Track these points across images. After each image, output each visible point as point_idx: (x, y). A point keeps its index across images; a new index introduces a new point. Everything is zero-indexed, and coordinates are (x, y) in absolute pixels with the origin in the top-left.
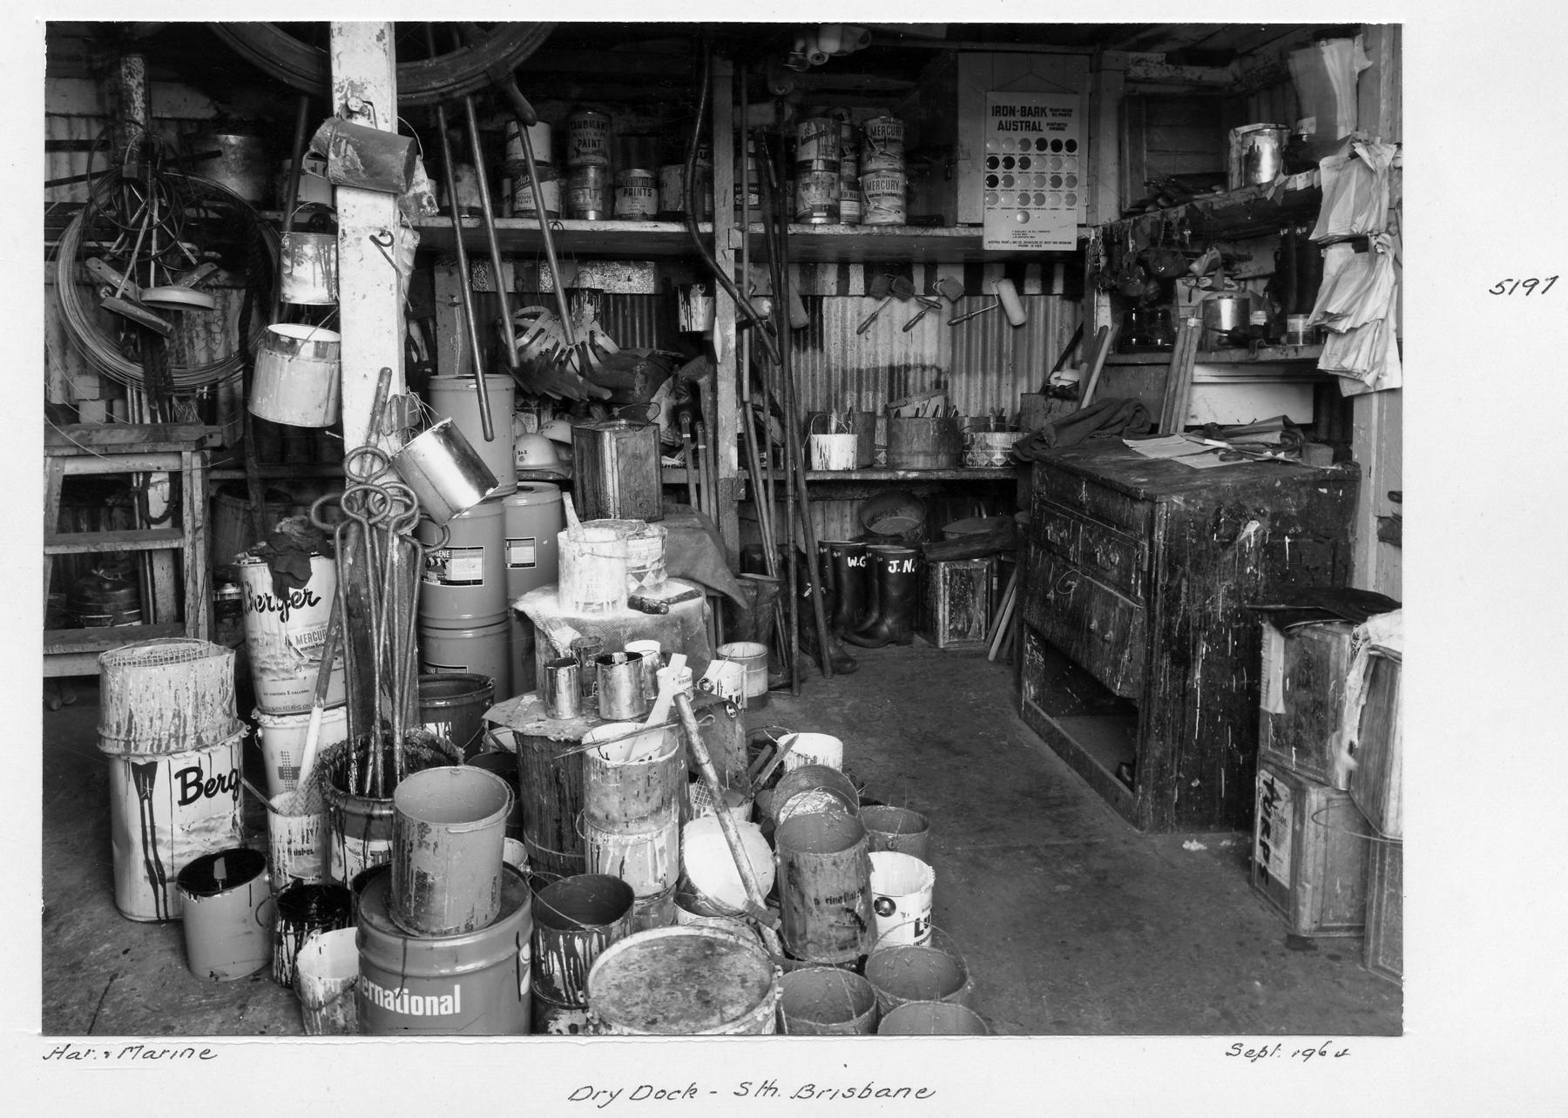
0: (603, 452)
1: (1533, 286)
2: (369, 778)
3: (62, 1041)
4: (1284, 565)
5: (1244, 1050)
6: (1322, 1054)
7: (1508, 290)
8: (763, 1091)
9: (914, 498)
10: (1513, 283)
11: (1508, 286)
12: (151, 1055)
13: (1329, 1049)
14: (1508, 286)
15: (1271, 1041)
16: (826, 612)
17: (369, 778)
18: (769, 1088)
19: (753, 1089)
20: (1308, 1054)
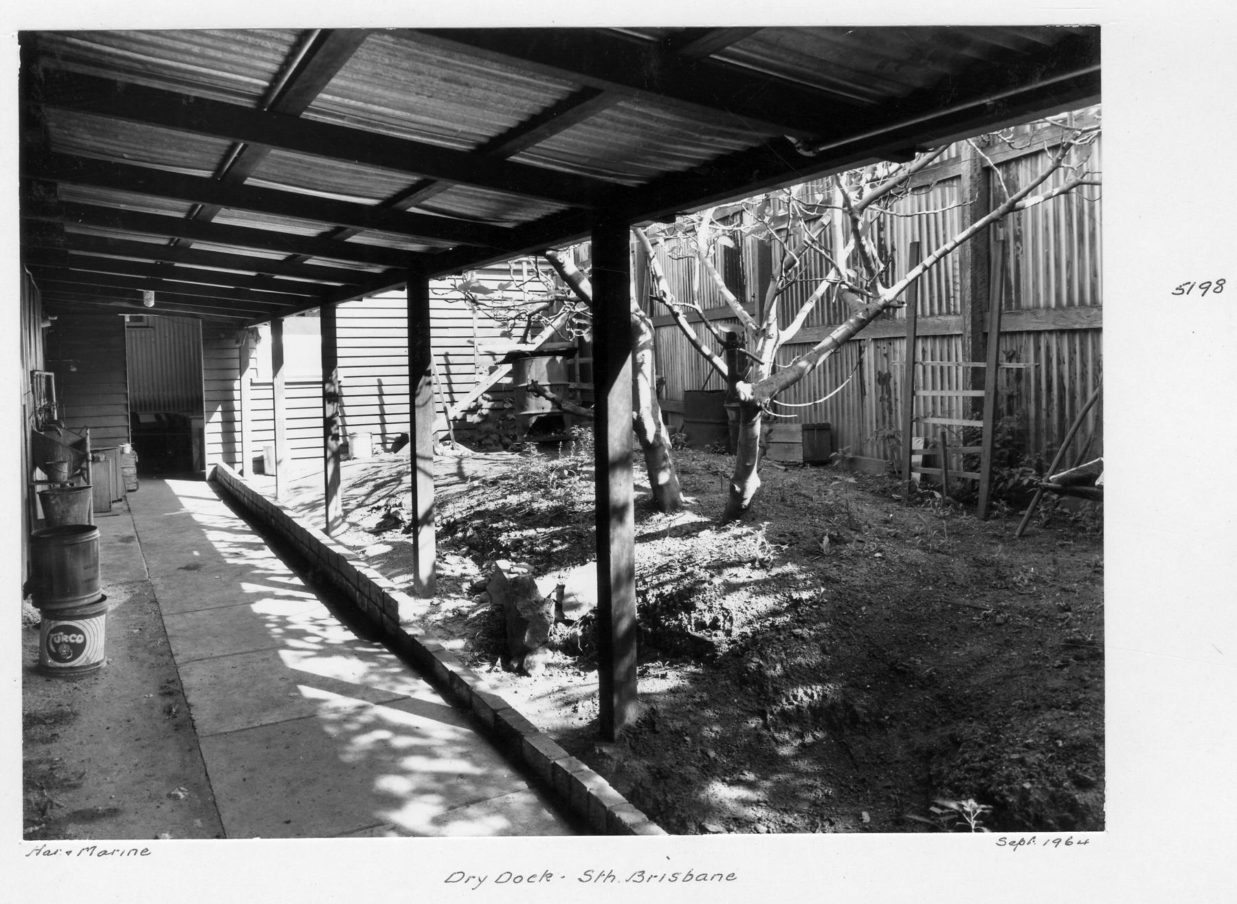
0: (466, 185)
1: (1208, 288)
2: (398, 113)
3: (39, 843)
4: (42, 828)
5: (1008, 841)
6: (1067, 843)
7: (1186, 291)
8: (602, 878)
9: (886, 271)
10: (1189, 286)
11: (1186, 288)
12: (48, 853)
13: (1075, 840)
14: (1186, 288)
15: (1027, 835)
16: (1009, 253)
17: (398, 113)
18: (548, 875)
19: (680, 878)
20: (1057, 842)
